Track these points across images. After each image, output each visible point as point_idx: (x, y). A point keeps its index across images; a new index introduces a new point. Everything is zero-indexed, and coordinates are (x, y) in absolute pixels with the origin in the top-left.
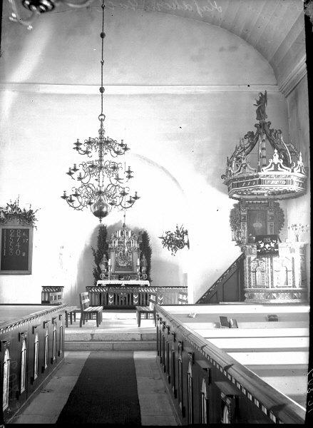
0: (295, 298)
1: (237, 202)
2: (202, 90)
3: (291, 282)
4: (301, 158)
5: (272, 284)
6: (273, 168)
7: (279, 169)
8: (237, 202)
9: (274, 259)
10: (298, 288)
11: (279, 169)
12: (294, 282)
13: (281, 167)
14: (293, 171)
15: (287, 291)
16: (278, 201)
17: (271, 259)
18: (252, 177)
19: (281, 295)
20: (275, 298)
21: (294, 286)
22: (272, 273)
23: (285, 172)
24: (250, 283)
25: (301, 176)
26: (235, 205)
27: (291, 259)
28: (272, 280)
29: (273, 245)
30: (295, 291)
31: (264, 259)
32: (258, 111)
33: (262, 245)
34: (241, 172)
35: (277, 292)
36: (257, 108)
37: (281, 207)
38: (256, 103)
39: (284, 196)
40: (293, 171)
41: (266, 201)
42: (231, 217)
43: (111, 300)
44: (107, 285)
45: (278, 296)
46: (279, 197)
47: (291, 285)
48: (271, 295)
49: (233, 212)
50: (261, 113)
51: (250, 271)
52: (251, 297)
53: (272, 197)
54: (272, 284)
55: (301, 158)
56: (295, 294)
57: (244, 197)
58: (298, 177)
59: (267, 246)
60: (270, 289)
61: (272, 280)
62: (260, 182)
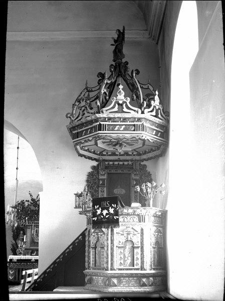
0: (144, 285)
1: (95, 163)
2: (60, 36)
3: (139, 262)
4: (157, 97)
5: (112, 264)
6: (116, 109)
7: (125, 110)
8: (95, 163)
9: (116, 230)
10: (149, 271)
11: (125, 110)
12: (142, 262)
13: (127, 106)
14: (143, 113)
15: (132, 275)
16: (144, 163)
17: (112, 231)
18: (91, 122)
19: (124, 280)
20: (116, 286)
21: (142, 268)
22: (112, 249)
23: (134, 113)
24: (89, 263)
25: (157, 120)
26: (93, 168)
27: (139, 231)
28: (112, 260)
29: (112, 211)
30: (144, 276)
31: (103, 229)
32: (115, 52)
33: (99, 212)
34: (116, 109)
35: (119, 277)
36: (114, 47)
37: (149, 169)
38: (113, 43)
39: (150, 155)
40: (143, 113)
41: (130, 163)
42: (87, 181)
43: (12, 275)
44: (18, 260)
45: (120, 282)
46: (144, 157)
47: (139, 267)
48: (110, 282)
49: (90, 175)
50: (118, 52)
51: (89, 246)
52: (90, 281)
53: (137, 158)
54: (112, 264)
55: (157, 97)
56: (144, 280)
57: (104, 158)
58: (153, 123)
59: (105, 212)
60: (109, 272)
61: (112, 260)
62: (100, 127)
